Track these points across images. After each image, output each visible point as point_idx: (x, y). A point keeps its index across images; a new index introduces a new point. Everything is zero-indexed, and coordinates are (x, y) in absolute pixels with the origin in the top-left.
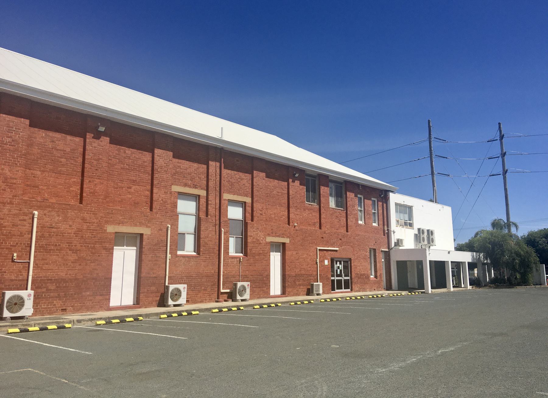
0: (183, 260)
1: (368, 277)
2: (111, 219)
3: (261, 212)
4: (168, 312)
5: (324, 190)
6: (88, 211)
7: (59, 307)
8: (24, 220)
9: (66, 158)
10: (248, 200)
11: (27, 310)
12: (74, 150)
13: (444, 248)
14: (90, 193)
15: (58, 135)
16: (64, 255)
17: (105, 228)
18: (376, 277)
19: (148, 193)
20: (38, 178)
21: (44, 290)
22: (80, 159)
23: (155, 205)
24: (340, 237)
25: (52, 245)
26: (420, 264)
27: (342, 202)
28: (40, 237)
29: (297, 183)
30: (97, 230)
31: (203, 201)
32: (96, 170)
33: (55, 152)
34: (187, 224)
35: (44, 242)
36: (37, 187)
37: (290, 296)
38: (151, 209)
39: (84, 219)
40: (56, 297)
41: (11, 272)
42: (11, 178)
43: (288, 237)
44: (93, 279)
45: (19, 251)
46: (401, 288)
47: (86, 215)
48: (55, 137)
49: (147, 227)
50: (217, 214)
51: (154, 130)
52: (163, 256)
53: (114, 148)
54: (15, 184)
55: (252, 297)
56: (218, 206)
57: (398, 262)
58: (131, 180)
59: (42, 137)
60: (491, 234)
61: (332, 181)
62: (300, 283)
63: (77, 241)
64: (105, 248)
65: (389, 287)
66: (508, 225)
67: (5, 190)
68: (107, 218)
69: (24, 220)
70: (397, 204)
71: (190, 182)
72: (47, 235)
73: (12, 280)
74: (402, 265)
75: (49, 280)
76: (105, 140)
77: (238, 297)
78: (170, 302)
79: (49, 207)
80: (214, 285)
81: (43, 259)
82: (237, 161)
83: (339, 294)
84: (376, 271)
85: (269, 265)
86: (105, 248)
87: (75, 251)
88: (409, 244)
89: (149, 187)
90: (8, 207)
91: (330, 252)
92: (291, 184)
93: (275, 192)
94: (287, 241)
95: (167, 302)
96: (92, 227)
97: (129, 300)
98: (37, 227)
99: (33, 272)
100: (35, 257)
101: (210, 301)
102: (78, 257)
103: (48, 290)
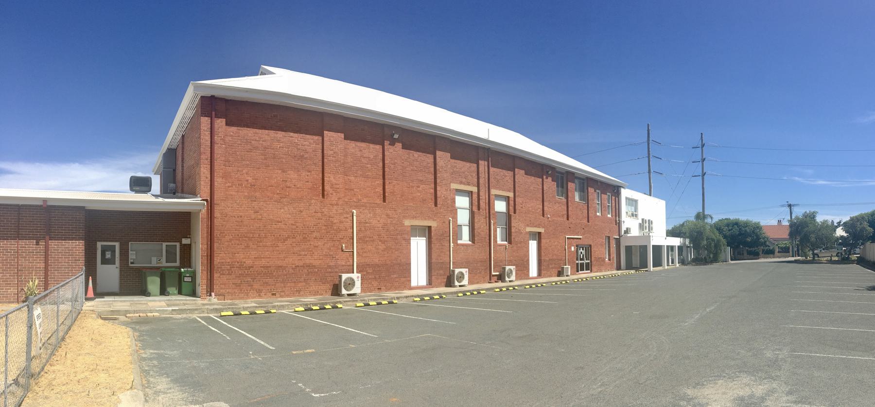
1: (604, 260)
5: (571, 186)
10: (511, 195)
11: (357, 289)
13: (659, 237)
15: (363, 145)
18: (609, 260)
19: (432, 191)
22: (381, 164)
23: (439, 200)
26: (644, 249)
27: (585, 198)
29: (550, 179)
31: (475, 196)
34: (463, 217)
35: (362, 235)
38: (436, 205)
39: (388, 215)
46: (629, 267)
47: (389, 212)
49: (434, 220)
52: (447, 245)
57: (626, 247)
60: (695, 225)
61: (577, 178)
65: (619, 268)
66: (705, 217)
70: (627, 198)
72: (363, 229)
74: (629, 249)
76: (399, 145)
77: (507, 279)
78: (457, 283)
79: (363, 206)
83: (584, 275)
84: (609, 255)
85: (528, 251)
87: (384, 242)
88: (635, 232)
89: (433, 186)
92: (545, 180)
94: (542, 230)
95: (454, 283)
97: (423, 282)
101: (484, 282)
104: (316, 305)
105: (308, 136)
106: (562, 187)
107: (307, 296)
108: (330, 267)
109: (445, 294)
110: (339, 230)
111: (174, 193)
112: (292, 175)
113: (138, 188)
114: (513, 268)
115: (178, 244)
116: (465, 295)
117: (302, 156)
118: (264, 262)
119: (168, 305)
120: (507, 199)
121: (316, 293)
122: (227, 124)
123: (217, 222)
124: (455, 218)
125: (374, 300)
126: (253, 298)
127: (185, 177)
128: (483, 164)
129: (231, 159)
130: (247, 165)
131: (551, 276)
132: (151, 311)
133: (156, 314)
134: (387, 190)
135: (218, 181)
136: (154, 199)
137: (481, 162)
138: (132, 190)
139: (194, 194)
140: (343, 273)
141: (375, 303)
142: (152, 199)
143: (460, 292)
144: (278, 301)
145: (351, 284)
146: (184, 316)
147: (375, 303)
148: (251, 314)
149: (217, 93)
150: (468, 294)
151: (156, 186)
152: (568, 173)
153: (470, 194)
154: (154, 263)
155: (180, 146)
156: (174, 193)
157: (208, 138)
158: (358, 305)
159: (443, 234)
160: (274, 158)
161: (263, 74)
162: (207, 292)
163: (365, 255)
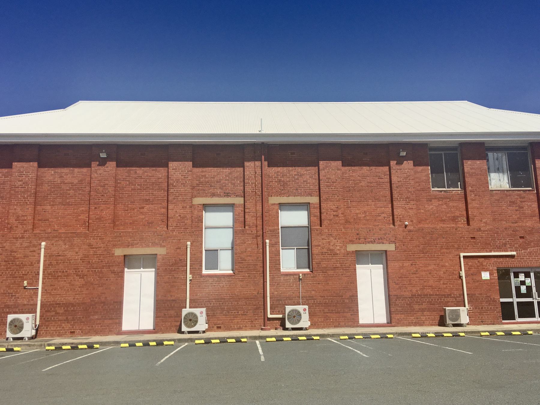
0: (211, 280)
2: (119, 243)
3: (335, 213)
4: (351, 334)
6: (94, 237)
7: (67, 330)
8: (34, 251)
9: (74, 190)
10: (314, 200)
12: (81, 181)
14: (96, 219)
15: (65, 170)
16: (71, 281)
17: (113, 252)
20: (49, 212)
21: (53, 313)
24: (522, 233)
25: (60, 272)
28: (48, 265)
30: (104, 255)
31: (240, 210)
32: (102, 195)
33: (63, 186)
35: (51, 270)
36: (48, 220)
37: (401, 326)
39: (90, 245)
40: (65, 320)
41: (24, 298)
42: (23, 216)
43: (390, 242)
44: (102, 303)
45: (30, 279)
47: (92, 241)
48: (63, 173)
49: (161, 246)
50: (259, 222)
51: (168, 144)
53: (123, 171)
54: (26, 220)
55: (314, 325)
56: (259, 214)
58: (143, 200)
59: (52, 175)
62: (424, 306)
63: (84, 266)
64: (113, 272)
67: (17, 227)
68: (114, 241)
69: (34, 251)
71: (219, 191)
72: (54, 262)
73: (25, 305)
75: (58, 304)
76: (112, 165)
80: (257, 309)
81: (51, 285)
82: (292, 154)
83: (519, 325)
86: (113, 272)
87: (82, 277)
90: (20, 241)
91: (493, 260)
94: (391, 247)
96: (99, 252)
98: (500, 251)
99: (42, 297)
100: (43, 283)
102: (86, 282)
103: (57, 313)
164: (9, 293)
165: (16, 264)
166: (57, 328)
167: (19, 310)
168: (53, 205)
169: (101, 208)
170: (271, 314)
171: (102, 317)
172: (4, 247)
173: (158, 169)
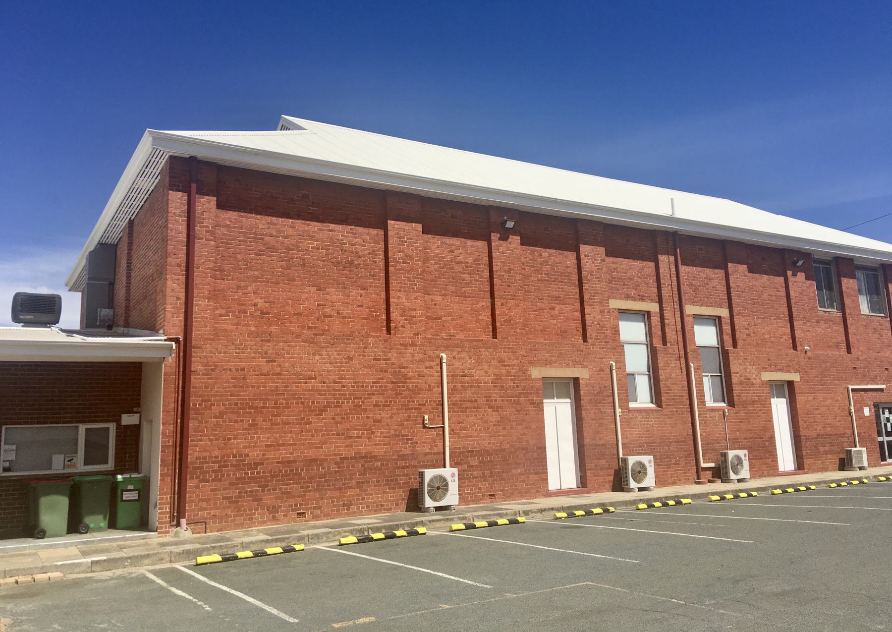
5: (848, 284)
8: (431, 368)
10: (724, 313)
11: (452, 498)
15: (456, 241)
19: (578, 315)
22: (486, 273)
24: (886, 365)
29: (801, 276)
31: (655, 320)
34: (636, 359)
35: (457, 398)
36: (440, 319)
38: (585, 339)
39: (501, 361)
42: (410, 309)
43: (796, 371)
44: (523, 449)
47: (504, 355)
52: (610, 411)
54: (415, 316)
55: (753, 476)
71: (633, 292)
72: (459, 386)
73: (426, 454)
76: (515, 240)
77: (732, 476)
78: (633, 484)
79: (457, 346)
80: (689, 455)
81: (459, 422)
87: (496, 409)
90: (410, 350)
91: (870, 393)
92: (791, 279)
93: (765, 296)
94: (795, 377)
95: (627, 484)
96: (513, 372)
97: (570, 480)
101: (687, 481)
104: (377, 530)
105: (360, 229)
106: (830, 288)
107: (361, 513)
108: (402, 457)
109: (612, 504)
110: (417, 390)
111: (109, 327)
112: (334, 294)
113: (30, 317)
114: (742, 453)
115: (112, 427)
116: (651, 506)
117: (351, 263)
118: (284, 453)
119: (85, 554)
120: (717, 321)
121: (378, 508)
122: (220, 206)
123: (195, 381)
124: (621, 361)
125: (483, 517)
126: (263, 523)
127: (135, 294)
128: (665, 260)
129: (226, 267)
130: (257, 277)
131: (824, 469)
132: (44, 570)
133: (56, 575)
134: (498, 317)
135: (201, 305)
136: (63, 338)
137: (663, 258)
138: (16, 318)
139: (151, 328)
140: (426, 467)
141: (485, 524)
142: (64, 336)
143: (642, 501)
144: (309, 528)
145: (441, 487)
146: (119, 572)
147: (485, 524)
148: (256, 555)
149: (200, 153)
150: (658, 504)
151: (72, 311)
152: (838, 259)
153: (646, 316)
154: (58, 465)
155: (126, 239)
156: (110, 327)
157: (183, 228)
158: (455, 526)
159: (600, 393)
160: (304, 266)
161: (284, 128)
162: (172, 518)
163: (463, 433)
164: (402, 436)
165: (408, 387)
166: (472, 489)
167: (419, 462)
168: (445, 295)
169: (509, 305)
170: (107, 463)
171: (526, 470)
172: (389, 359)
173: (566, 253)
